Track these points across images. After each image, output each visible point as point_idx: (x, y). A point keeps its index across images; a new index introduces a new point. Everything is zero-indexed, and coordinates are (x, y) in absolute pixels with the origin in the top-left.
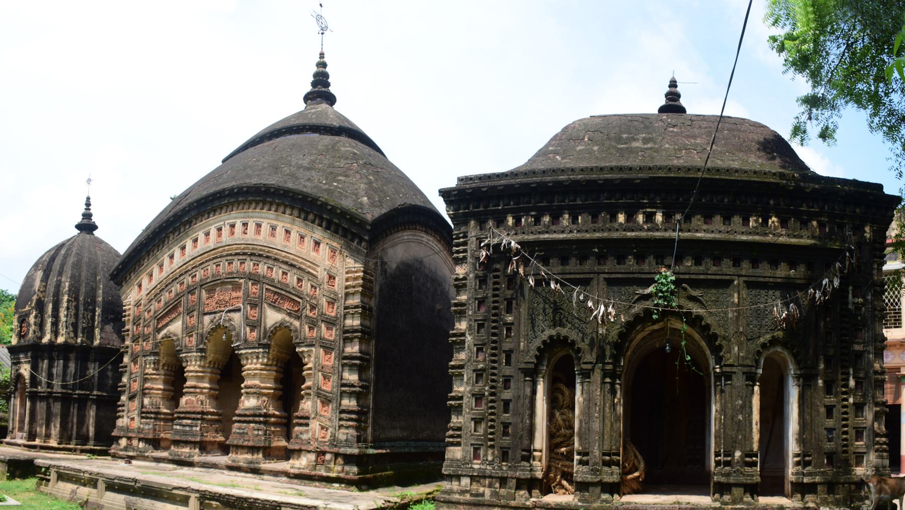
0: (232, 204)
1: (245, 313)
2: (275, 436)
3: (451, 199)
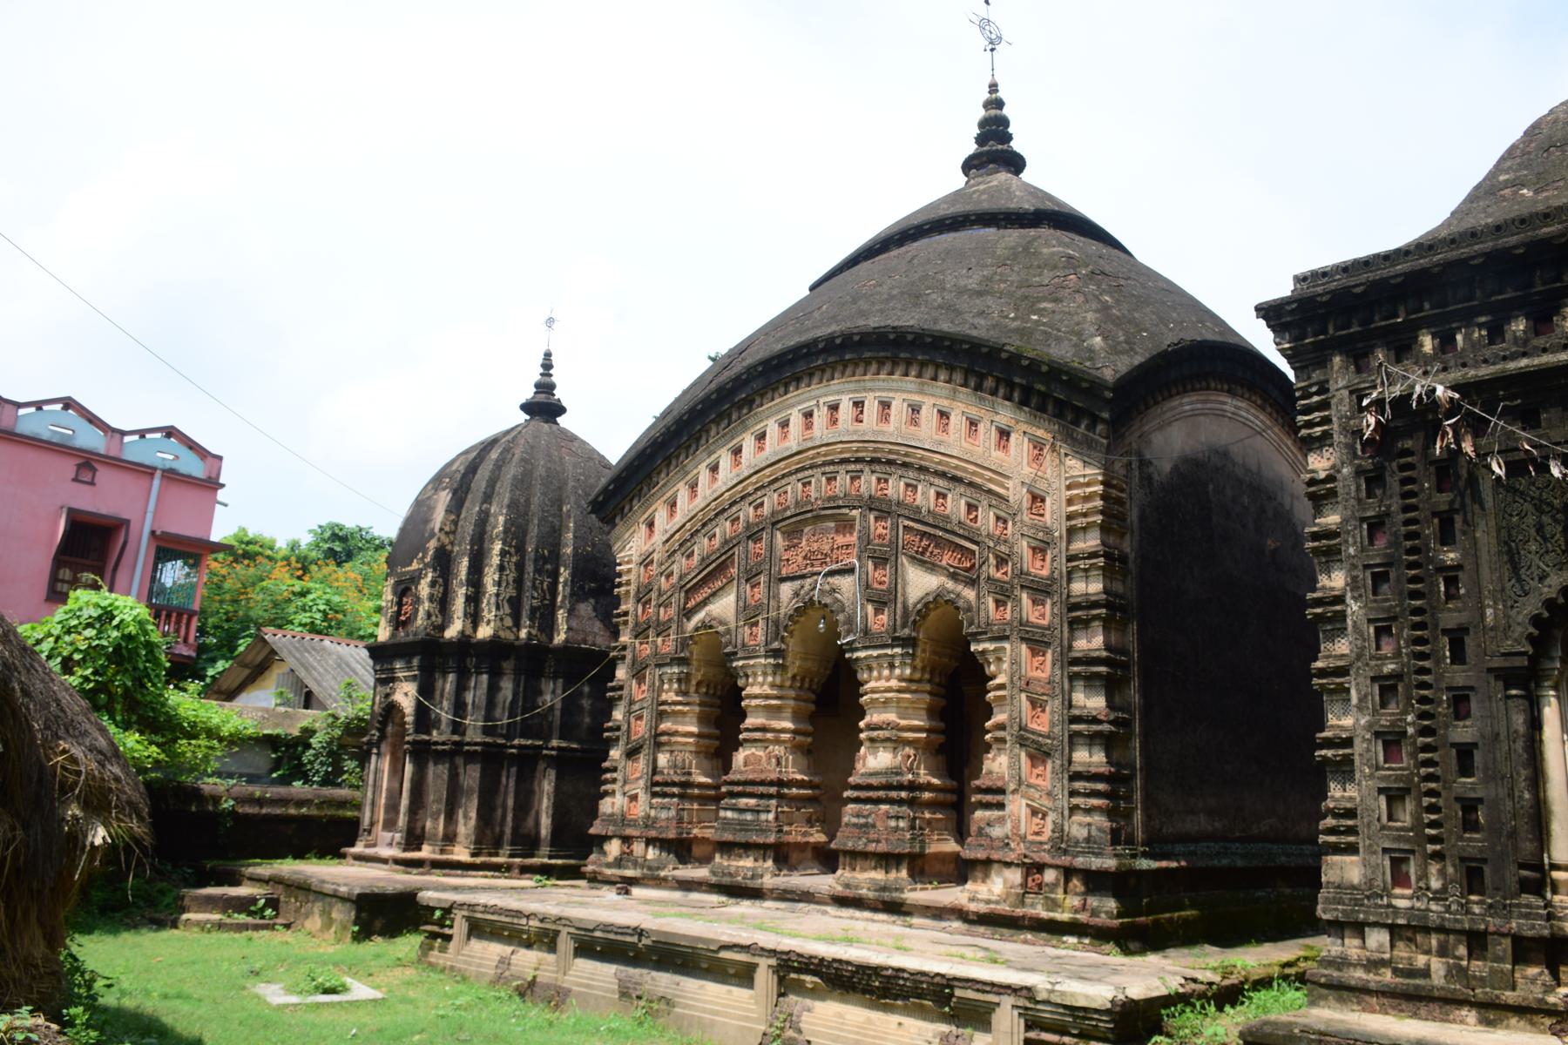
0: (833, 368)
1: (864, 576)
2: (932, 831)
3: (1284, 320)
